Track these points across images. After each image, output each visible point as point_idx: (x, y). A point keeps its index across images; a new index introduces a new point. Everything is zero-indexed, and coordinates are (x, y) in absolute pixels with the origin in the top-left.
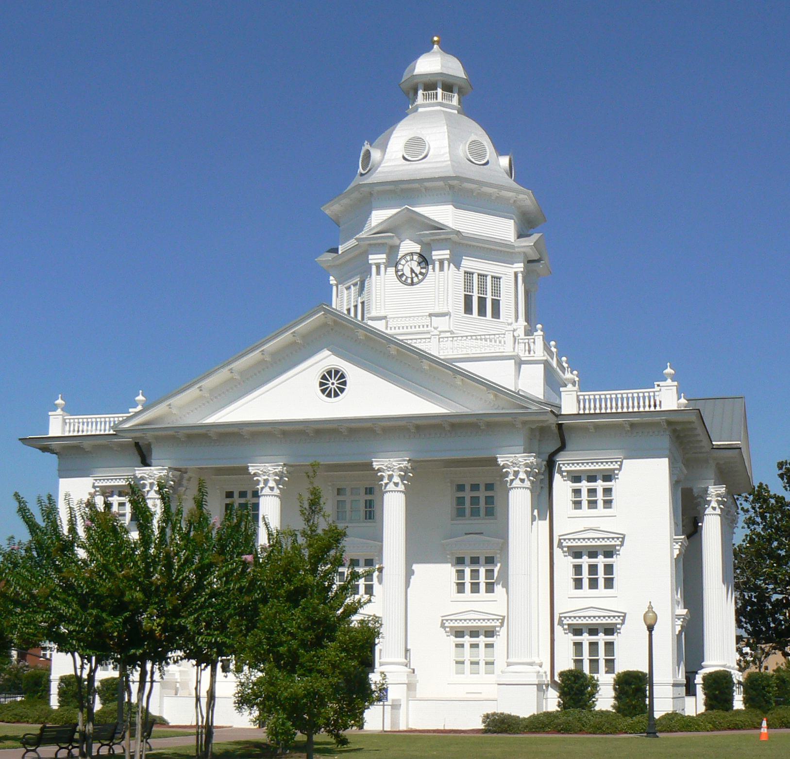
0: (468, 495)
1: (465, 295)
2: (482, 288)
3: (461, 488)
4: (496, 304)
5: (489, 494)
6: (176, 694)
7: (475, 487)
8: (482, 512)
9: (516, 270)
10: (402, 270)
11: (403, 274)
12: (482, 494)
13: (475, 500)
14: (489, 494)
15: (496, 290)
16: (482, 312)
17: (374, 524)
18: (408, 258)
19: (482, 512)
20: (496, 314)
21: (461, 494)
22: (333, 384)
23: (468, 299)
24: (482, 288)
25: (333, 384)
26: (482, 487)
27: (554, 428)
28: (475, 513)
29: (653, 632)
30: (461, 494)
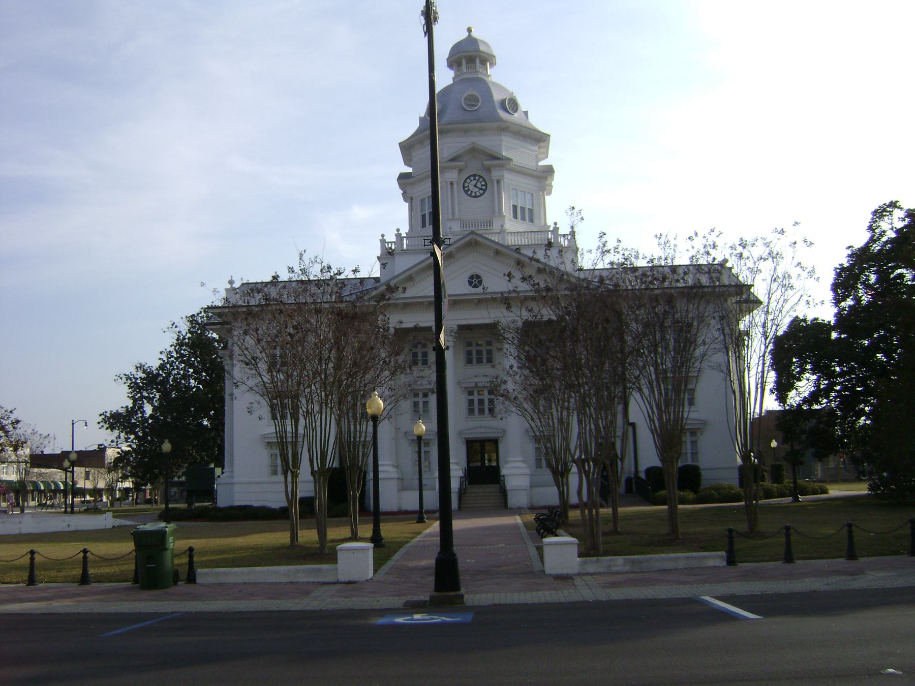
0: (474, 349)
12: (484, 349)
13: (479, 353)
23: (515, 207)
28: (480, 361)
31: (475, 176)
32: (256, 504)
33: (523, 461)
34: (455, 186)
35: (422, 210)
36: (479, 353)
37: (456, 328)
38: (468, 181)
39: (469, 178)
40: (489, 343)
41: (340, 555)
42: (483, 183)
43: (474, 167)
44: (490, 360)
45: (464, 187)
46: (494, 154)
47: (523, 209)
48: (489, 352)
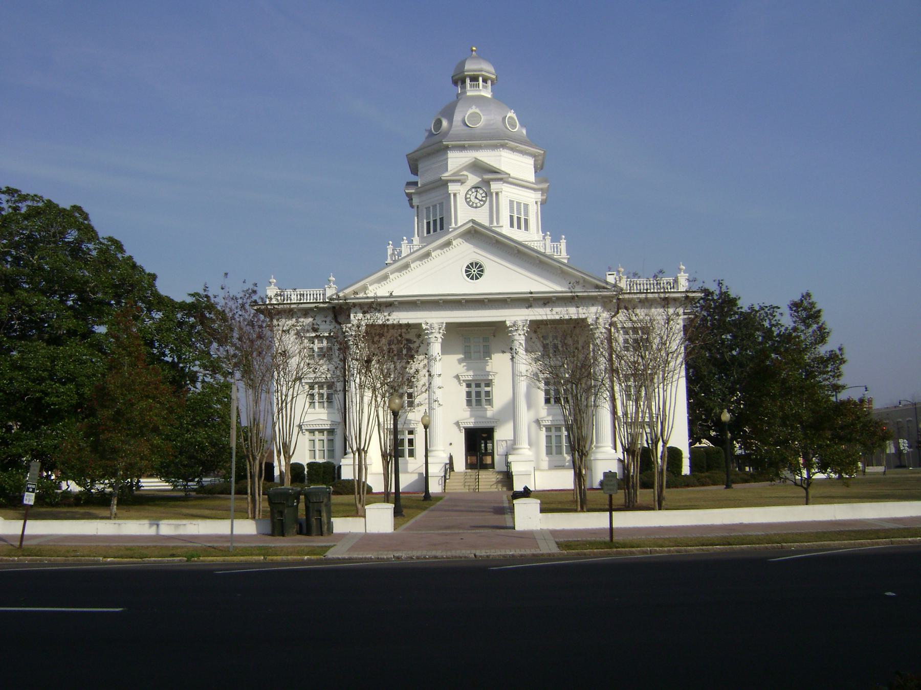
2: (519, 212)
4: (526, 221)
15: (526, 214)
16: (519, 227)
20: (526, 228)
22: (475, 271)
23: (511, 217)
24: (519, 212)
45: (466, 199)
47: (519, 219)
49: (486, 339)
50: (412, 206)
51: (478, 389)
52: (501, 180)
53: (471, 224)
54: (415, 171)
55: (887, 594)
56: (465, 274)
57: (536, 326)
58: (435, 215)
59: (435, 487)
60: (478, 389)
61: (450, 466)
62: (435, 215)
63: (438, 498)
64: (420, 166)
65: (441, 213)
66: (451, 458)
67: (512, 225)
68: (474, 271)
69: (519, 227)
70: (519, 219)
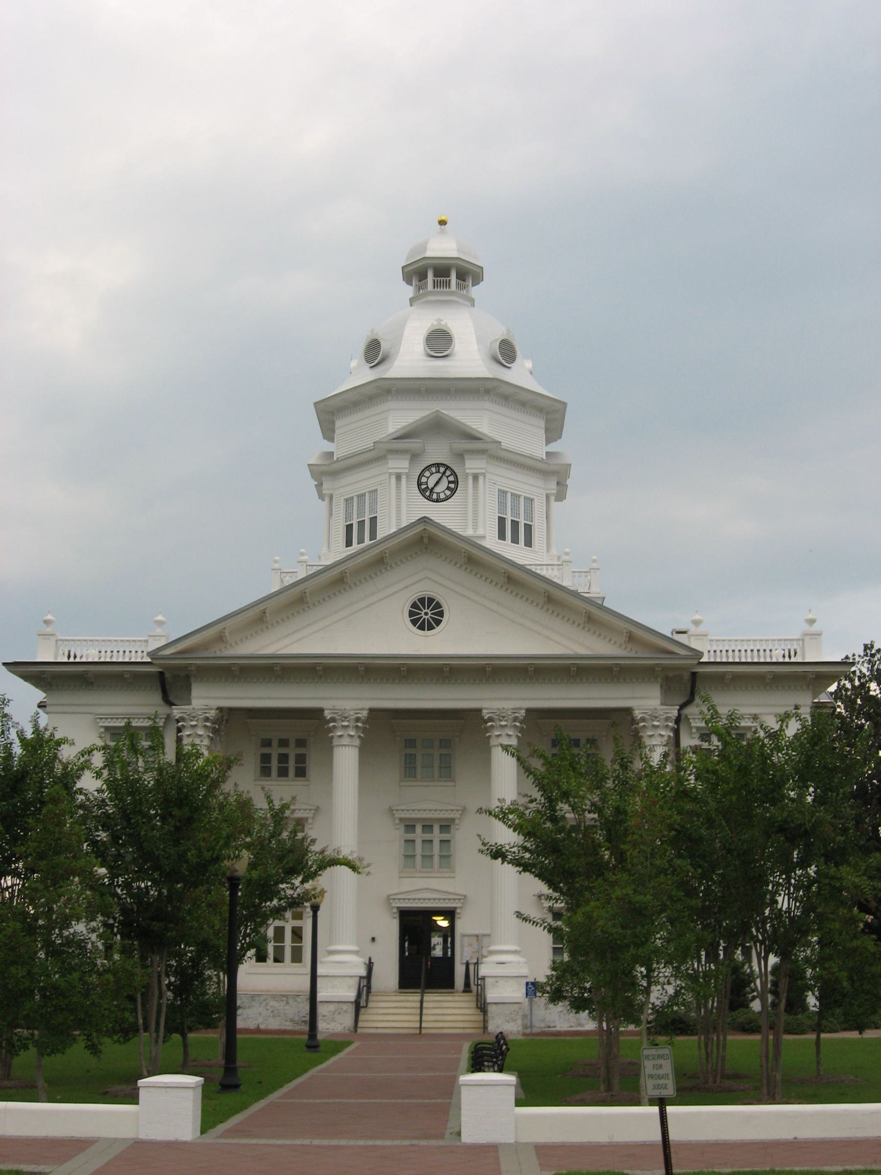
0: (275, 752)
1: (499, 517)
2: (515, 511)
3: (267, 743)
4: (528, 528)
5: (301, 751)
6: (489, 935)
7: (284, 743)
8: (292, 772)
9: (549, 492)
10: (427, 483)
11: (448, 488)
12: (292, 752)
13: (283, 758)
14: (301, 751)
15: (529, 514)
16: (515, 540)
17: (306, 783)
18: (434, 470)
19: (292, 772)
20: (529, 543)
21: (266, 751)
22: (426, 614)
23: (502, 521)
24: (515, 511)
25: (426, 614)
26: (275, 743)
27: (687, 676)
28: (283, 773)
29: (319, 913)
30: (266, 751)
31: (438, 465)
32: (601, 1170)
33: (356, 953)
34: (404, 480)
35: (348, 515)
36: (283, 758)
37: (365, 713)
38: (427, 474)
39: (428, 468)
40: (301, 743)
41: (142, 1093)
42: (452, 478)
43: (437, 451)
44: (301, 773)
45: (419, 484)
46: (474, 433)
47: (515, 524)
48: (301, 759)
49: (446, 744)
50: (321, 497)
51: (284, 751)
52: (483, 452)
53: (420, 528)
54: (329, 432)
55: (722, 957)
56: (426, 633)
57: (536, 718)
58: (361, 513)
59: (331, 1024)
60: (284, 751)
61: (366, 984)
62: (361, 513)
63: (337, 1045)
64: (338, 424)
65: (372, 510)
66: (370, 966)
67: (502, 536)
68: (426, 614)
69: (515, 540)
70: (515, 524)
